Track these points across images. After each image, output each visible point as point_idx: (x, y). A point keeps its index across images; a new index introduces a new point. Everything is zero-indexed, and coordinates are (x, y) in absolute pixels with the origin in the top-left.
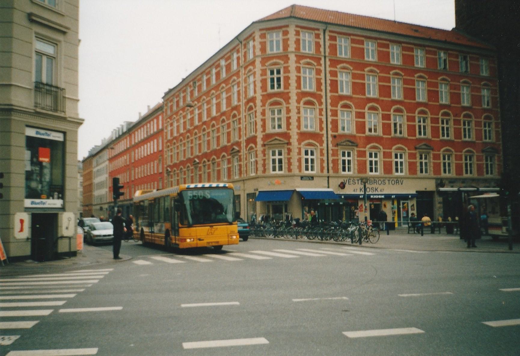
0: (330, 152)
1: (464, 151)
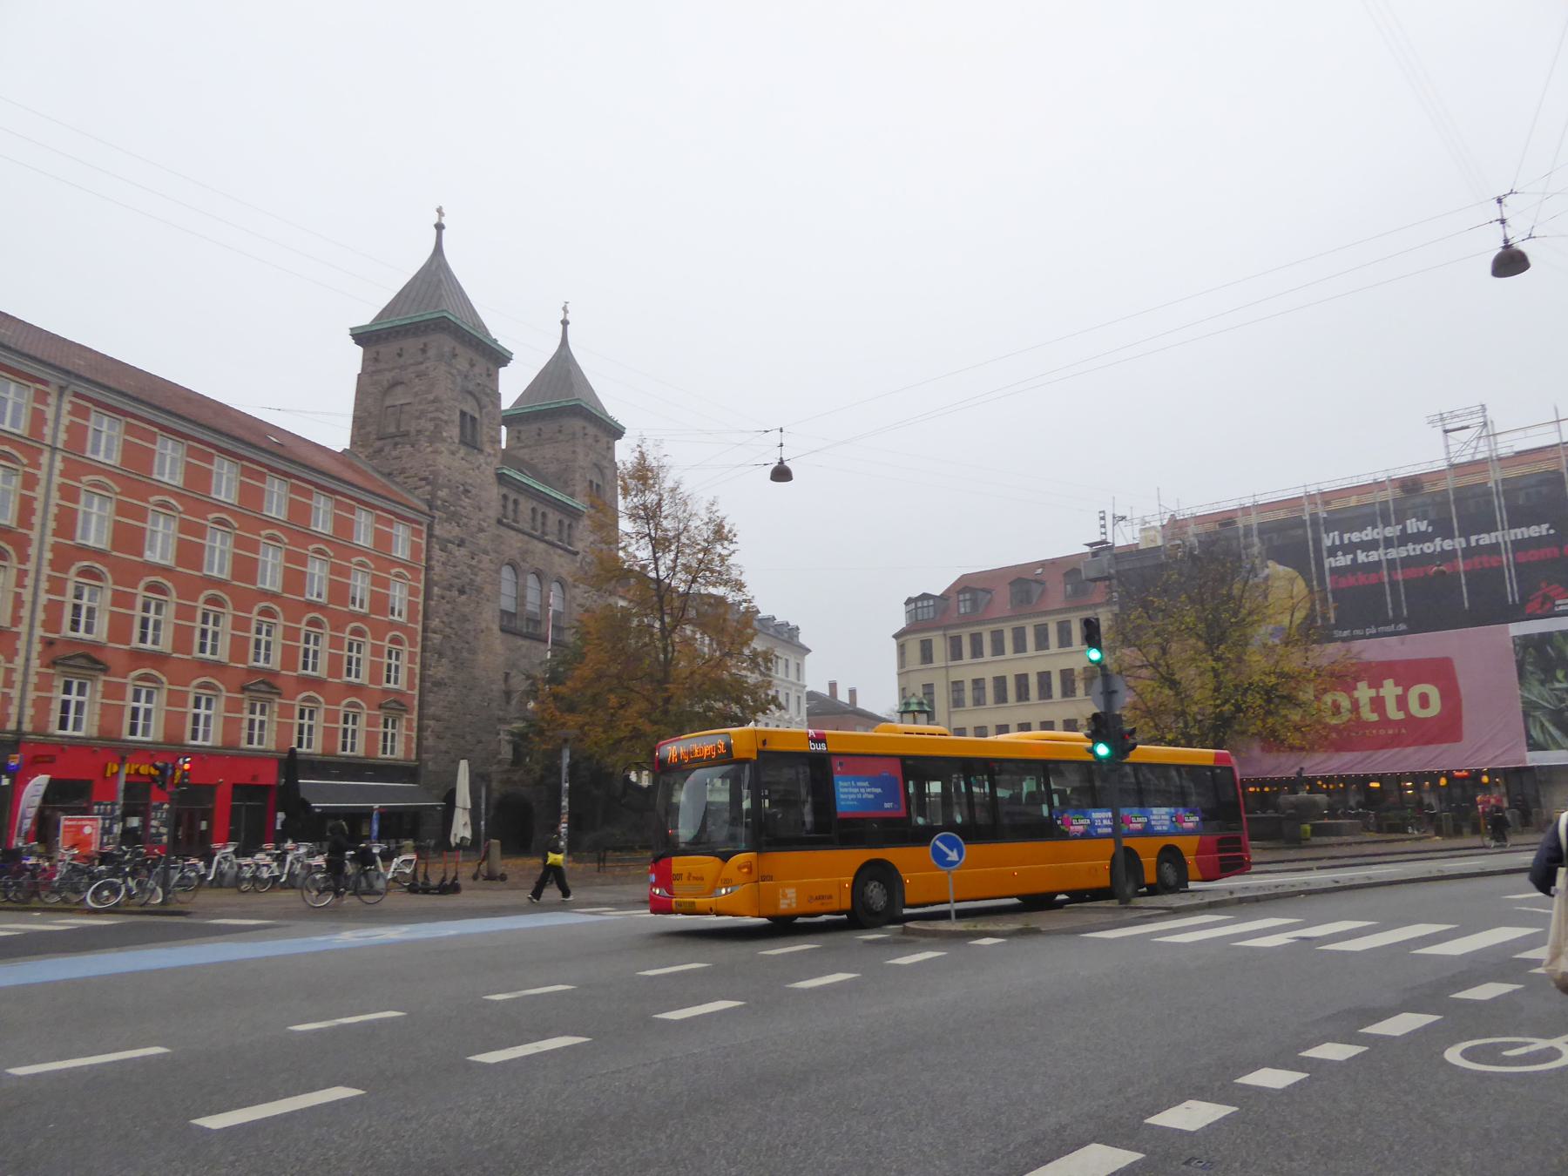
0: (33, 679)
1: (195, 682)
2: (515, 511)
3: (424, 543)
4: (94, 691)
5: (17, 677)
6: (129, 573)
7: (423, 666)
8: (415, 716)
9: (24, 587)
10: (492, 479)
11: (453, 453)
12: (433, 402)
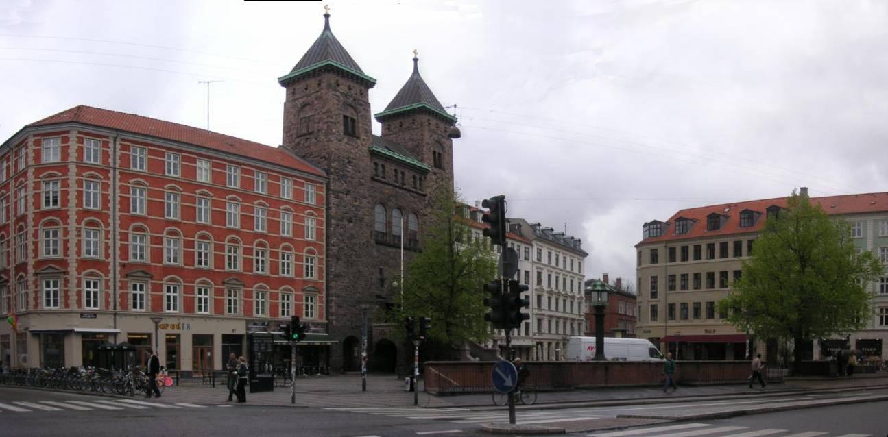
0: (118, 284)
2: (384, 172)
3: (324, 194)
4: (147, 288)
5: (111, 284)
6: (220, 235)
7: (327, 266)
8: (324, 294)
9: (109, 239)
10: (366, 154)
11: (340, 141)
12: (326, 113)
